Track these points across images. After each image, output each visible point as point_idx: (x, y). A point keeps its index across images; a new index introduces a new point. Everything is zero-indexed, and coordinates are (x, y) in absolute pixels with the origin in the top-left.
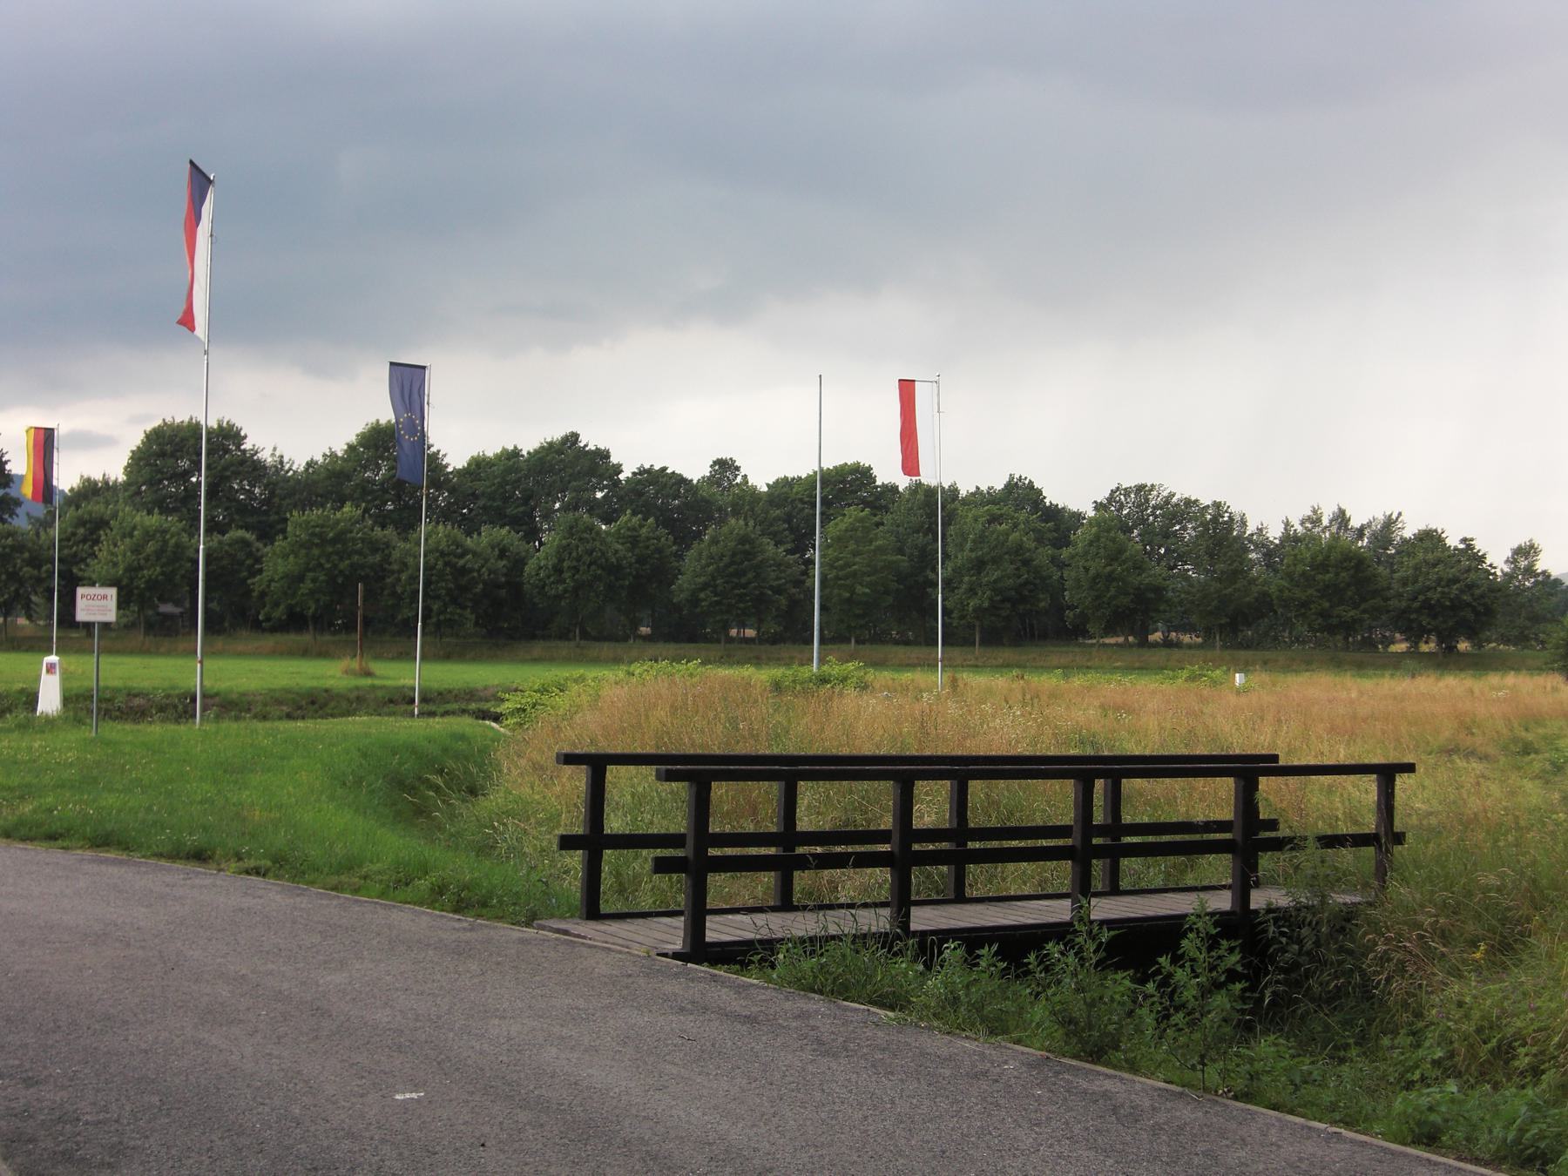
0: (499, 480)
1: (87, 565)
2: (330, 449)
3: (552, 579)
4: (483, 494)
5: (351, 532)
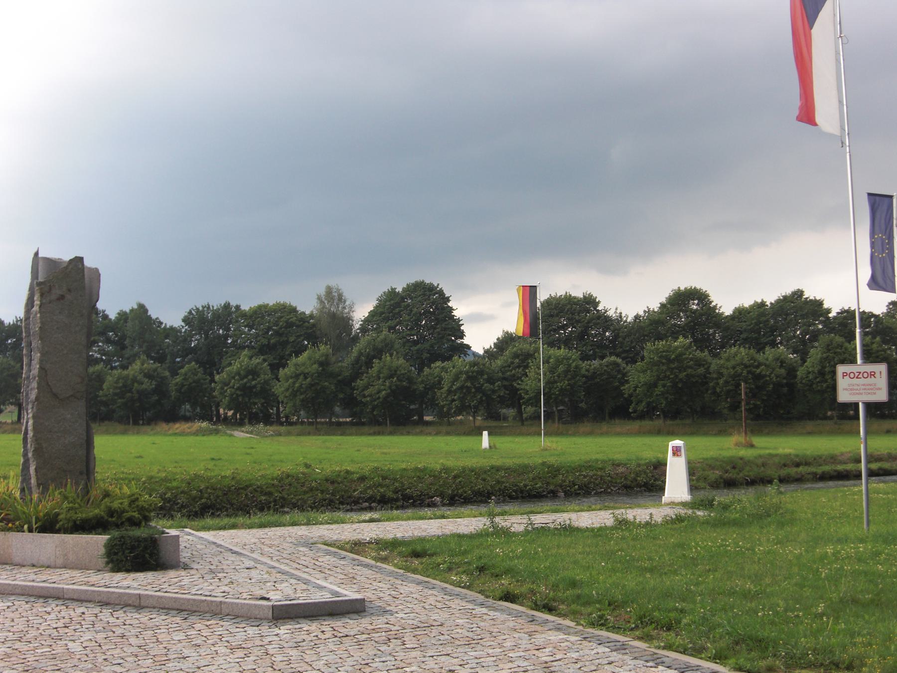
0: (755, 321)
1: (522, 381)
2: (648, 307)
3: (818, 380)
4: (745, 330)
5: (684, 355)
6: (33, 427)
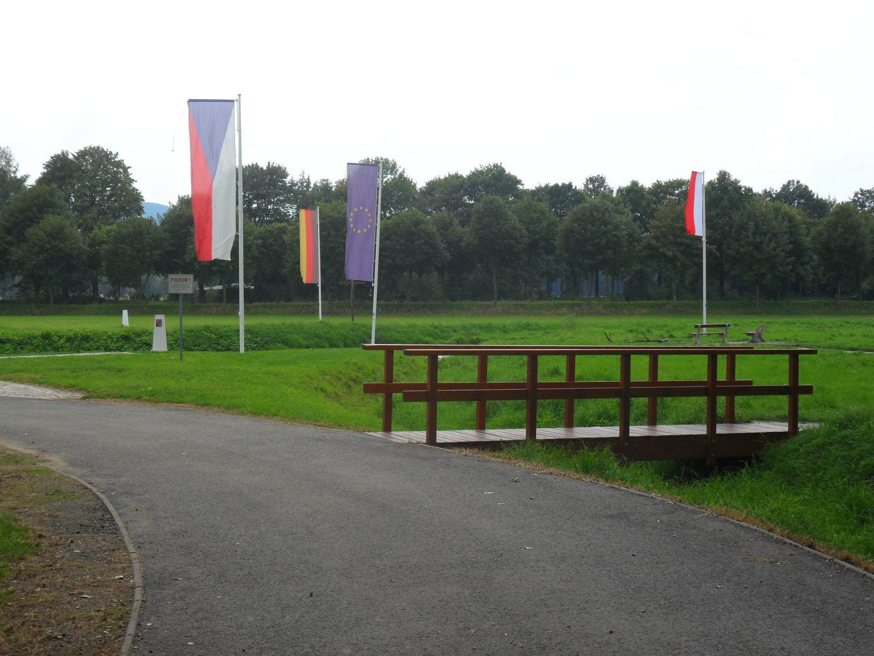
2: (501, 163)
6: (391, 422)
